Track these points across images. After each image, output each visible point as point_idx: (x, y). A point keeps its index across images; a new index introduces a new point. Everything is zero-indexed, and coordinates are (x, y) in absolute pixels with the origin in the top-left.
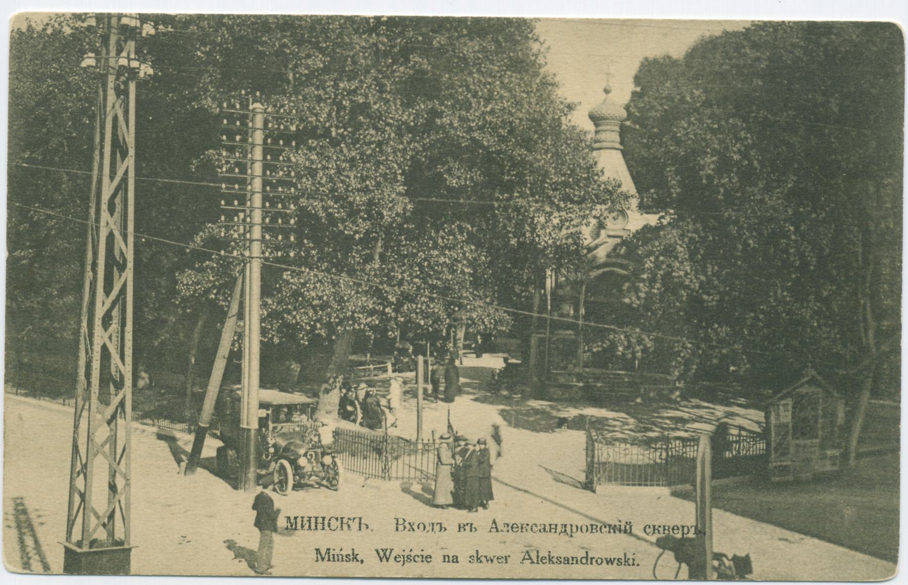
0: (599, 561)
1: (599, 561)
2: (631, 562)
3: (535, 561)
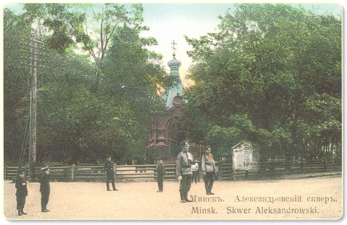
1: (297, 211)
3: (261, 212)
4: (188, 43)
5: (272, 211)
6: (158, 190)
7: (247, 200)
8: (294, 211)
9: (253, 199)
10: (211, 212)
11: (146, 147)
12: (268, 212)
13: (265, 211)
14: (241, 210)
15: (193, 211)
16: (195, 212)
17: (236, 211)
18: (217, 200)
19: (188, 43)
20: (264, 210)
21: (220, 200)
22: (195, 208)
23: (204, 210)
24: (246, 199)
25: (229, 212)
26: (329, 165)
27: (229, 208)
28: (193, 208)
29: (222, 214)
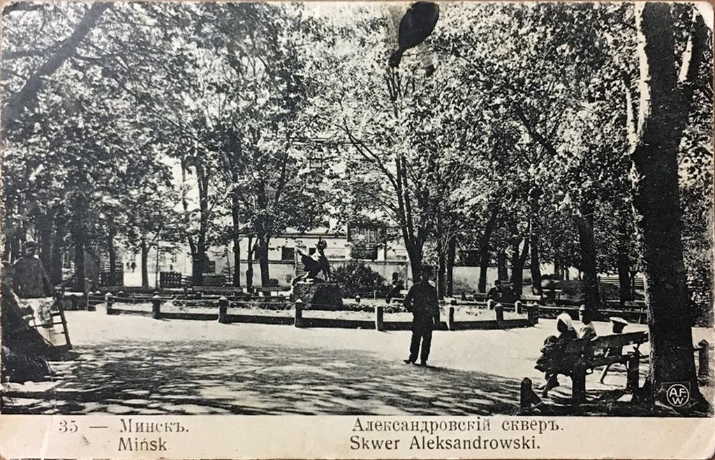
0: (494, 444)
1: (494, 444)
2: (530, 444)
3: (421, 446)
4: (173, 176)
5: (444, 444)
6: (408, 359)
7: (379, 428)
8: (488, 444)
9: (391, 426)
10: (522, 446)
11: (195, 155)
13: (428, 443)
14: (380, 443)
15: (122, 447)
16: (125, 448)
17: (370, 445)
18: (174, 428)
19: (173, 176)
21: (555, 427)
23: (467, 444)
24: (376, 425)
25: (355, 446)
26: (698, 408)
28: (121, 439)
29: (404, 451)
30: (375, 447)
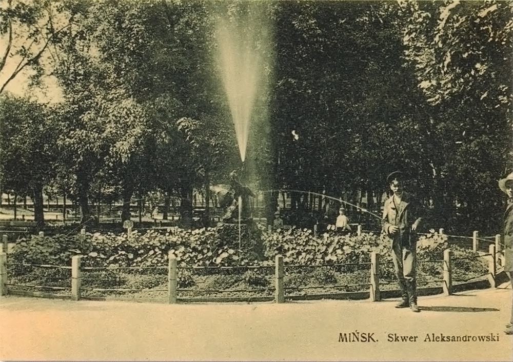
2: (496, 338)
12: (440, 339)
20: (435, 336)
22: (482, 340)
25: (391, 339)
27: (391, 336)
30: (403, 341)
